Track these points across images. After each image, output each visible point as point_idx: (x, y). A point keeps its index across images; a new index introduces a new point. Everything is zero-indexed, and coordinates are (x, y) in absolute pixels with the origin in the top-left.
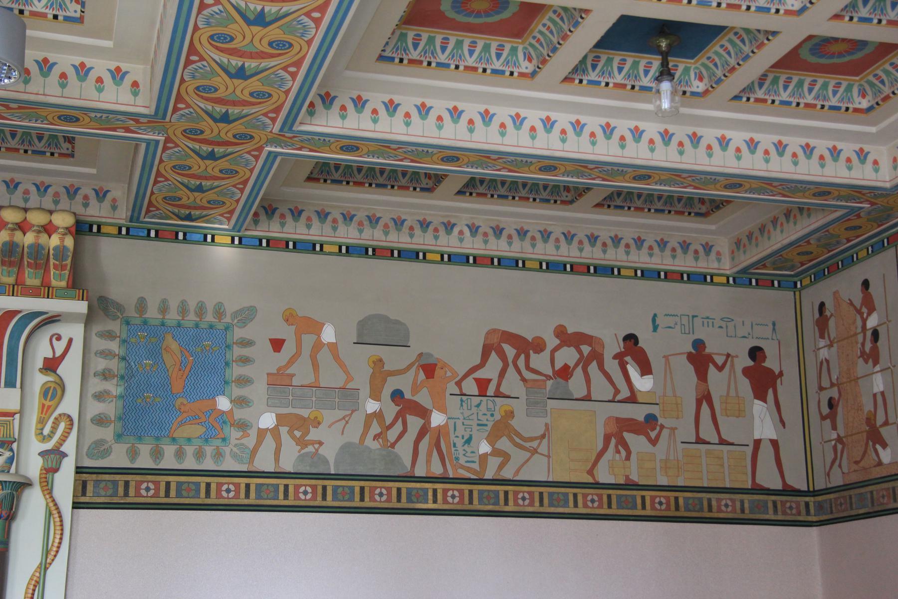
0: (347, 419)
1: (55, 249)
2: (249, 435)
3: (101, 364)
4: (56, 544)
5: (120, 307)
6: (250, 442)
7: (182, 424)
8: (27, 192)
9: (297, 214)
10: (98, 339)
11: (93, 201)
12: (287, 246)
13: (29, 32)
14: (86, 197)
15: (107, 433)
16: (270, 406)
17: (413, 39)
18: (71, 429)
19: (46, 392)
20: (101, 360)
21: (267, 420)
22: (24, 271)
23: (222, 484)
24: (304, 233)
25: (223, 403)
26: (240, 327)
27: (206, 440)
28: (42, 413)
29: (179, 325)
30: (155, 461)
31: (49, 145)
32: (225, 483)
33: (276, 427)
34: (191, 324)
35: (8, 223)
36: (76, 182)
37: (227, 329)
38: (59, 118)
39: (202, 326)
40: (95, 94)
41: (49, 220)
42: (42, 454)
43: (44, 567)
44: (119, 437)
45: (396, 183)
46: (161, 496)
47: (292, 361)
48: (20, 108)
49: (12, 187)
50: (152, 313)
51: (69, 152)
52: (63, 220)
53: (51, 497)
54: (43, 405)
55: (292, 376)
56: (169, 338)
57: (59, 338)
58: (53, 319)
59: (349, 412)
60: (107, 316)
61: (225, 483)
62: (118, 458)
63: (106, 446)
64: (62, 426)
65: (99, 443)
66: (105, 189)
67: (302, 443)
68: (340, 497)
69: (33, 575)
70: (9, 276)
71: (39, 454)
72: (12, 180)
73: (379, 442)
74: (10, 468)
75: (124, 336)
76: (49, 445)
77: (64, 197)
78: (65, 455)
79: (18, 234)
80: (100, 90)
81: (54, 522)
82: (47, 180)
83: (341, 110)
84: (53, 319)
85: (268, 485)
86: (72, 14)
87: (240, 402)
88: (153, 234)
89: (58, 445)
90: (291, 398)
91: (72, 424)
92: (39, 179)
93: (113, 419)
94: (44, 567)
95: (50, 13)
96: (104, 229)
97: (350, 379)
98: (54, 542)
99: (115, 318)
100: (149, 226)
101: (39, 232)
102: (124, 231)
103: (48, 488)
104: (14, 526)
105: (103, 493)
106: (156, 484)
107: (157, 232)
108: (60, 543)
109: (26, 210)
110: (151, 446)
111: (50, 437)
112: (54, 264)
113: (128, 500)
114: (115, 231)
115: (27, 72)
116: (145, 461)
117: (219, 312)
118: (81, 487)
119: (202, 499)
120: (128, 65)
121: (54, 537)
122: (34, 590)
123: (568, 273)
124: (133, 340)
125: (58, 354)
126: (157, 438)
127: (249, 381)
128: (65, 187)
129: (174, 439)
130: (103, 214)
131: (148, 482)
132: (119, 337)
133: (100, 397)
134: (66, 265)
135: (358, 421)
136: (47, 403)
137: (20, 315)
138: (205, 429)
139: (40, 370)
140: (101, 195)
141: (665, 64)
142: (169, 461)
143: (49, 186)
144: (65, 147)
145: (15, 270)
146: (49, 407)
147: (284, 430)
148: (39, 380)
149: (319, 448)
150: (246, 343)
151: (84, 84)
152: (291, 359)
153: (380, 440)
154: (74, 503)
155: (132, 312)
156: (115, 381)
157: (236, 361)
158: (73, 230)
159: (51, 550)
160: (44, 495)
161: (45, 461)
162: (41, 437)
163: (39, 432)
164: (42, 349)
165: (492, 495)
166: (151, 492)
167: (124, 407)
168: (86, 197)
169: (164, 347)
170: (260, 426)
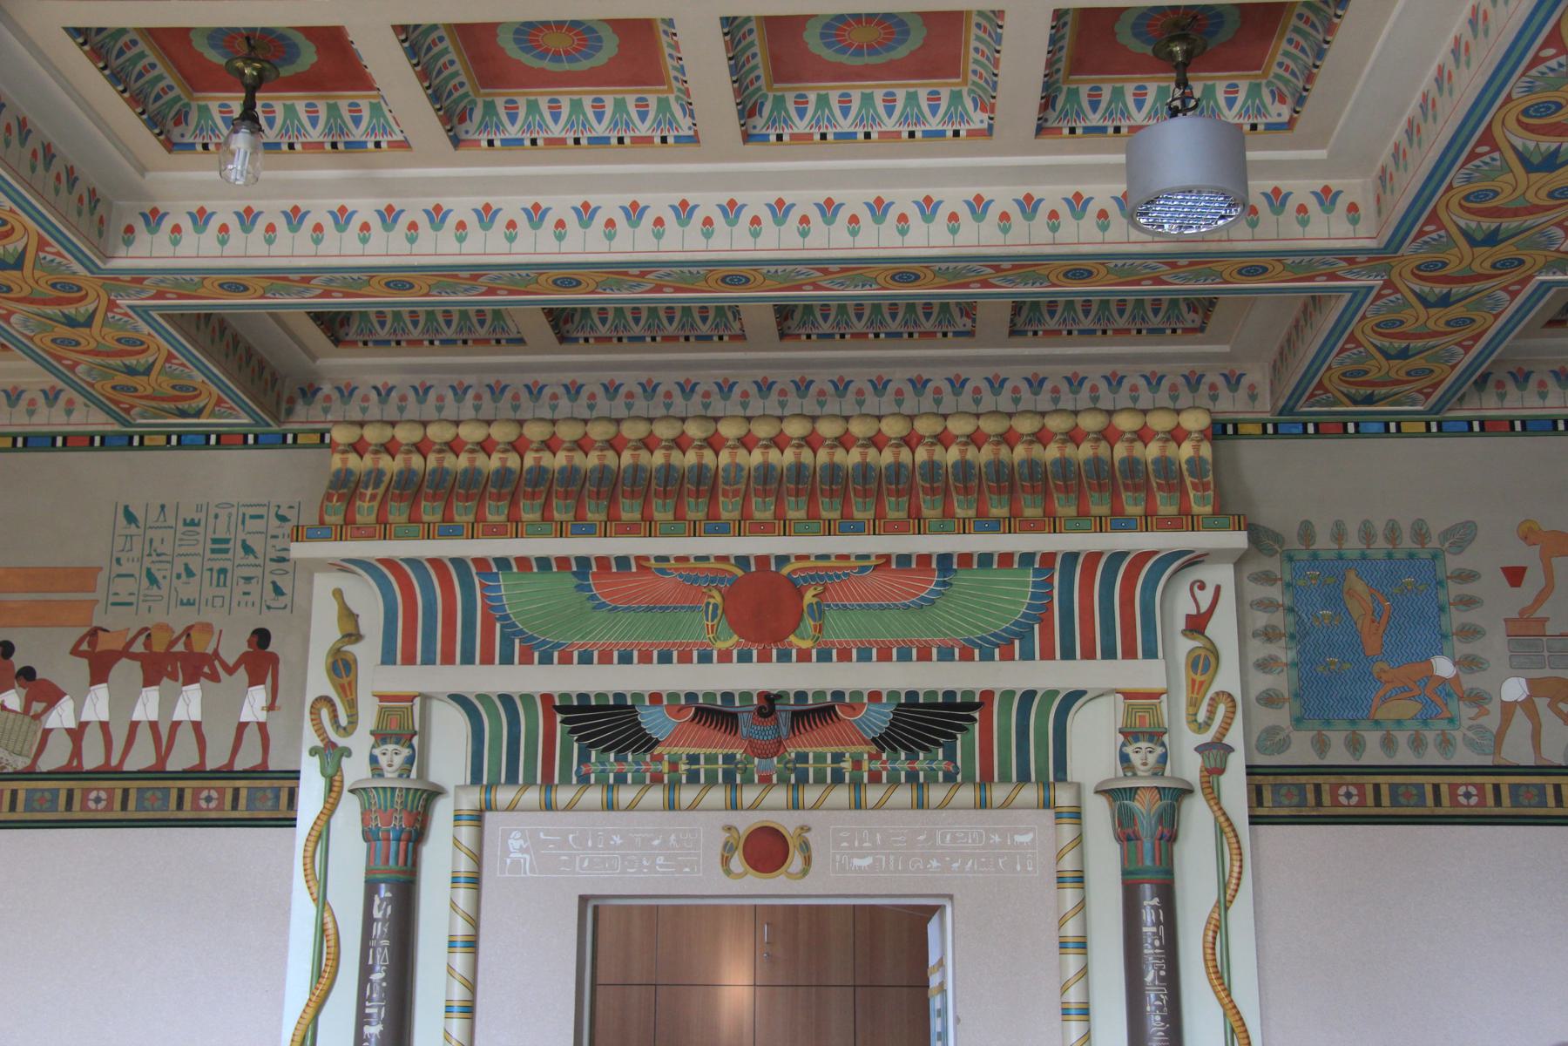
1: (1189, 461)
2: (1487, 713)
3: (1260, 619)
4: (1235, 875)
5: (1277, 538)
6: (1492, 722)
7: (1384, 700)
8: (1134, 388)
9: (1522, 378)
10: (1252, 584)
11: (1223, 390)
12: (1512, 427)
13: (1251, 155)
14: (1213, 387)
15: (1281, 717)
16: (1516, 668)
17: (1089, 96)
18: (1234, 713)
19: (1194, 663)
20: (1259, 613)
21: (1514, 689)
22: (1155, 497)
23: (1458, 786)
24: (1535, 405)
25: (1444, 667)
26: (1455, 554)
27: (1425, 722)
29: (1364, 557)
30: (1353, 754)
31: (1169, 318)
32: (1462, 784)
33: (1529, 699)
34: (1381, 555)
35: (1124, 433)
36: (1198, 367)
37: (1434, 557)
38: (1240, 272)
39: (1397, 556)
40: (1297, 230)
41: (1040, 426)
42: (1201, 749)
43: (1224, 905)
44: (1298, 721)
45: (1143, 326)
47: (1540, 599)
48: (1191, 264)
49: (1114, 383)
50: (1323, 542)
51: (969, 328)
52: (1195, 421)
53: (1221, 809)
54: (1194, 681)
55: (1544, 621)
56: (1352, 575)
57: (1202, 587)
58: (1195, 559)
60: (1260, 551)
61: (1462, 784)
62: (1301, 752)
63: (1281, 736)
64: (1221, 710)
65: (1272, 731)
66: (1238, 373)
69: (1210, 917)
70: (1136, 505)
71: (1196, 749)
72: (1114, 374)
74: (1164, 769)
75: (1287, 578)
76: (1207, 737)
77: (1184, 392)
78: (1230, 749)
79: (1037, 448)
80: (1304, 223)
81: (1229, 844)
82: (1159, 369)
83: (267, 230)
84: (1195, 559)
85: (1527, 785)
86: (978, 126)
87: (1468, 663)
88: (1311, 429)
90: (1546, 654)
91: (1235, 706)
92: (1148, 369)
93: (1286, 695)
94: (1224, 905)
95: (570, 137)
96: (1243, 429)
98: (1231, 871)
99: (1272, 553)
100: (1386, 418)
101: (1167, 440)
102: (1270, 429)
104: (1177, 848)
105: (1286, 802)
106: (1360, 787)
107: (1316, 426)
108: (1240, 873)
109: (554, 422)
110: (1344, 734)
111: (1207, 725)
112: (1193, 483)
113: (1323, 811)
114: (1257, 430)
115: (1254, 211)
116: (1339, 755)
117: (1420, 534)
118: (1256, 795)
119: (1429, 808)
120: (1339, 181)
121: (1232, 865)
122: (1214, 938)
123: (1518, 435)
124: (1301, 582)
126: (1353, 722)
127: (1478, 632)
128: (1184, 376)
129: (1377, 722)
130: (1239, 407)
131: (1347, 785)
132: (1281, 579)
133: (1265, 665)
134: (1208, 483)
136: (1199, 678)
137: (1156, 558)
138: (1420, 706)
139: (1184, 633)
140: (1233, 381)
141: (249, 106)
142: (1373, 755)
143: (1163, 377)
144: (962, 323)
145: (1143, 495)
146: (1202, 683)
147: (1542, 703)
148: (1185, 646)
150: (1467, 576)
151: (1281, 218)
154: (1250, 817)
155: (1294, 544)
156: (1282, 642)
157: (1454, 604)
158: (1209, 433)
159: (1229, 882)
160: (1211, 807)
162: (1195, 726)
163: (1192, 719)
164: (1184, 606)
165: (1535, 792)
166: (1354, 800)
167: (1300, 679)
168: (1213, 387)
169: (1346, 589)
170: (1505, 698)
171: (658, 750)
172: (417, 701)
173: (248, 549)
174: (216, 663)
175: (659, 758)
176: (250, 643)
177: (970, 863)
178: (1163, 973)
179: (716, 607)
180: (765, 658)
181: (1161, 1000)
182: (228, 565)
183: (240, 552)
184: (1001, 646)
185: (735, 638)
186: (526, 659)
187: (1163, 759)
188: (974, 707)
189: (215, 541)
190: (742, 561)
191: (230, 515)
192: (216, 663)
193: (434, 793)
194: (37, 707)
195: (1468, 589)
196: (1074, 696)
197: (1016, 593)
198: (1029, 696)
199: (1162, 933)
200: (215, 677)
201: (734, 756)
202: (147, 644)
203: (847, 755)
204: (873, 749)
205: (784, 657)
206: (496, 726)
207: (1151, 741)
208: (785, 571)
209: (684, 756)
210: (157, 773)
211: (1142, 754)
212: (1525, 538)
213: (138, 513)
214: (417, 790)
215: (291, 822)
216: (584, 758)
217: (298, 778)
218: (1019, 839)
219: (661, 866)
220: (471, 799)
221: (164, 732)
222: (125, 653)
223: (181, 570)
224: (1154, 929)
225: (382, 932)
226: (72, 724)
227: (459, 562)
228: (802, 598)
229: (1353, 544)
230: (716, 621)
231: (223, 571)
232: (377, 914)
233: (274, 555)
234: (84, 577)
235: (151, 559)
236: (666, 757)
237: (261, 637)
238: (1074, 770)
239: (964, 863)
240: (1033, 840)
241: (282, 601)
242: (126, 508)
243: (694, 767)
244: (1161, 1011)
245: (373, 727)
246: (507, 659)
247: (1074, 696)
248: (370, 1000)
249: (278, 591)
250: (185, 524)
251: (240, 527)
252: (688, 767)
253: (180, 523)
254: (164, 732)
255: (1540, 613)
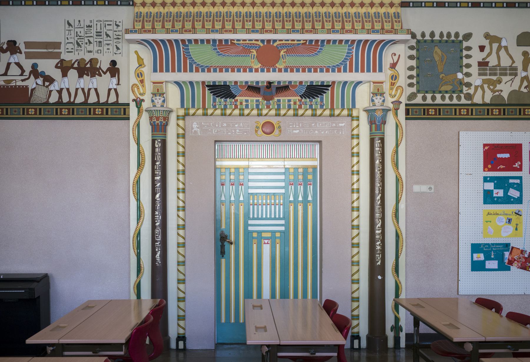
0: (513, 80)
2: (471, 89)
25: (460, 76)
28: (391, 86)
43: (397, 146)
46: (453, 115)
47: (489, 55)
54: (392, 83)
59: (514, 77)
67: (493, 91)
68: (80, 113)
73: (527, 89)
78: (401, 103)
84: (394, 42)
89: (398, 99)
97: (513, 62)
103: (396, 114)
111: (395, 96)
117: (457, 35)
125: (395, 62)
135: (518, 80)
147: (486, 86)
148: (390, 72)
149: (501, 93)
150: (469, 48)
152: (488, 54)
153: (528, 88)
161: (394, 105)
171: (236, 98)
172: (164, 83)
173: (108, 35)
174: (100, 70)
175: (237, 100)
176: (110, 64)
177: (327, 132)
178: (381, 161)
179: (254, 55)
180: (268, 71)
181: (380, 168)
182: (102, 40)
183: (105, 36)
184: (336, 69)
185: (260, 65)
186: (197, 71)
187: (384, 101)
188: (329, 86)
189: (97, 32)
190: (262, 41)
191: (101, 24)
192: (100, 70)
193: (171, 111)
194: (47, 84)
195: (453, 35)
196: (359, 83)
197: (342, 52)
198: (345, 83)
199: (381, 150)
200: (100, 75)
201: (259, 100)
202: (78, 64)
203: (292, 100)
204: (300, 98)
205: (274, 71)
206: (188, 91)
207: (381, 96)
208: (275, 45)
209: (244, 100)
210: (85, 103)
211: (378, 100)
212: (485, 37)
213: (72, 22)
214: (166, 110)
215: (128, 119)
216: (214, 101)
217: (129, 106)
218: (340, 125)
219: (238, 132)
220: (182, 112)
221: (86, 91)
222: (72, 67)
223: (87, 41)
224: (379, 149)
225: (158, 151)
226: (58, 89)
227: (176, 41)
228: (280, 52)
229: (437, 38)
230: (254, 59)
231: (100, 42)
232: (157, 146)
233: (116, 37)
234: (57, 45)
235: (77, 38)
236: (239, 101)
237: (114, 63)
238: (357, 106)
239: (325, 132)
240: (344, 125)
241: (119, 51)
242: (68, 21)
243: (247, 103)
244: (380, 171)
245: (152, 91)
246: (191, 71)
247: (359, 83)
248: (156, 170)
249: (118, 48)
250: (87, 27)
251: (104, 28)
252: (246, 103)
253: (85, 26)
254: (86, 91)
255: (487, 60)
